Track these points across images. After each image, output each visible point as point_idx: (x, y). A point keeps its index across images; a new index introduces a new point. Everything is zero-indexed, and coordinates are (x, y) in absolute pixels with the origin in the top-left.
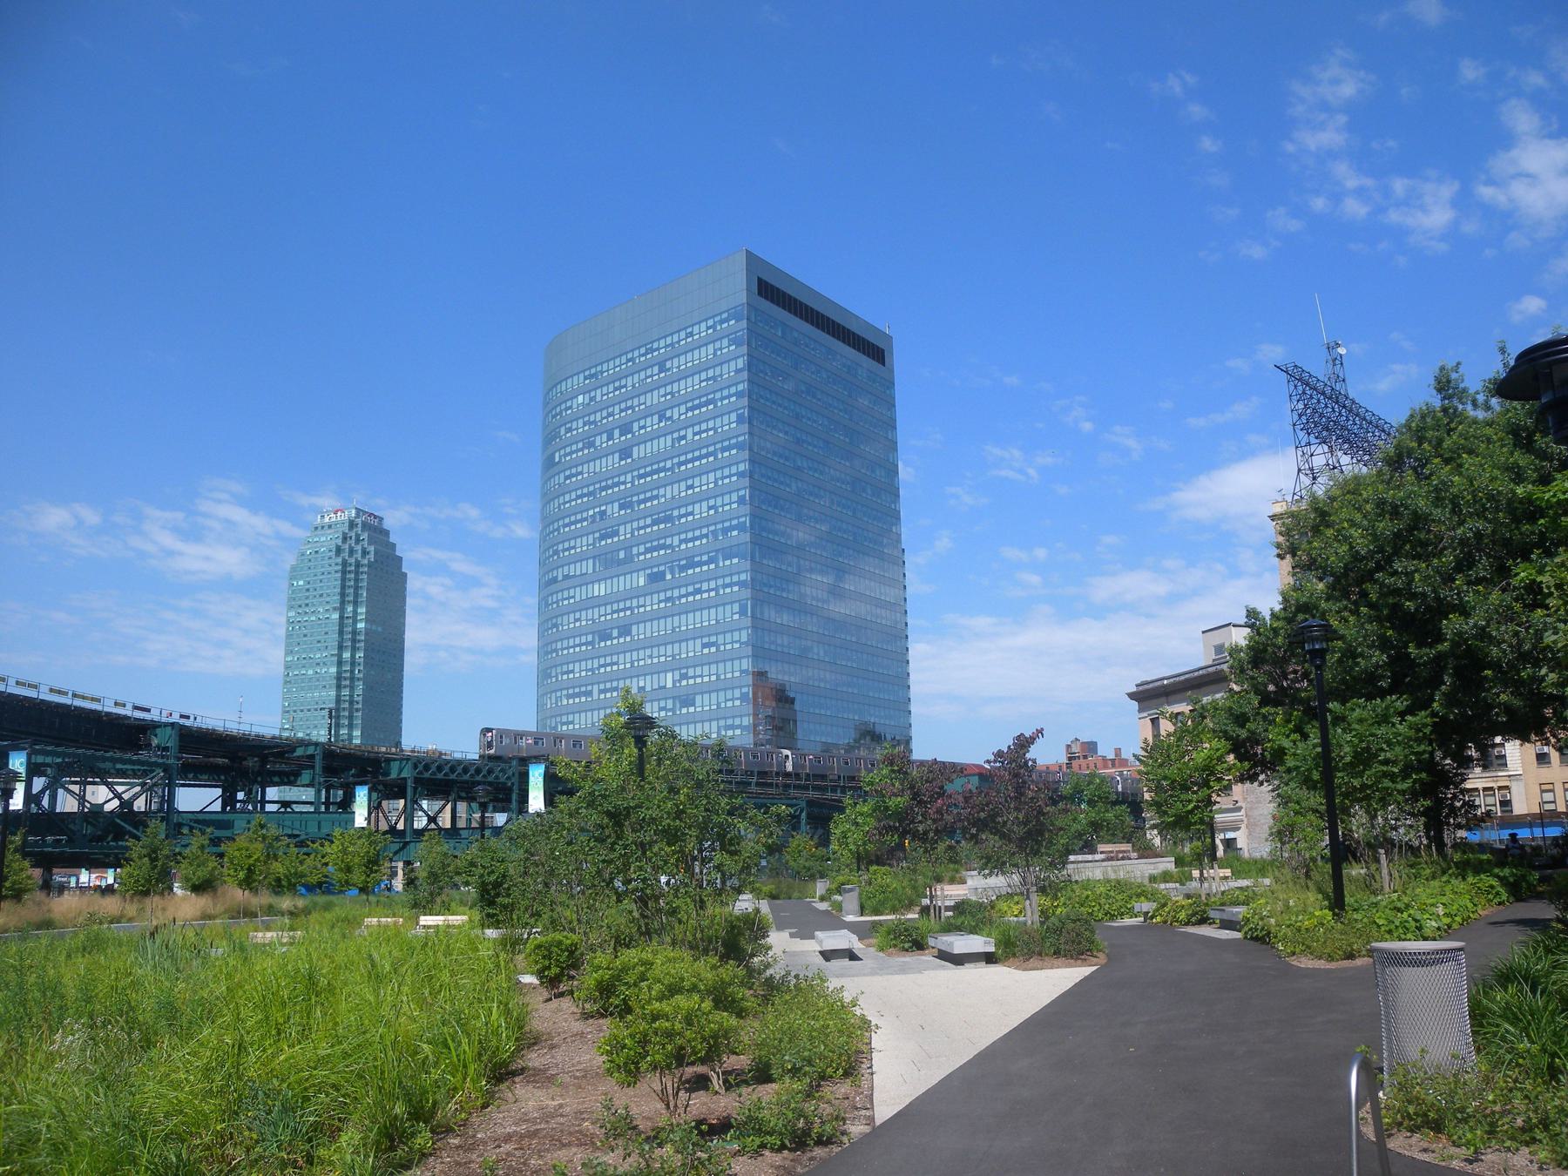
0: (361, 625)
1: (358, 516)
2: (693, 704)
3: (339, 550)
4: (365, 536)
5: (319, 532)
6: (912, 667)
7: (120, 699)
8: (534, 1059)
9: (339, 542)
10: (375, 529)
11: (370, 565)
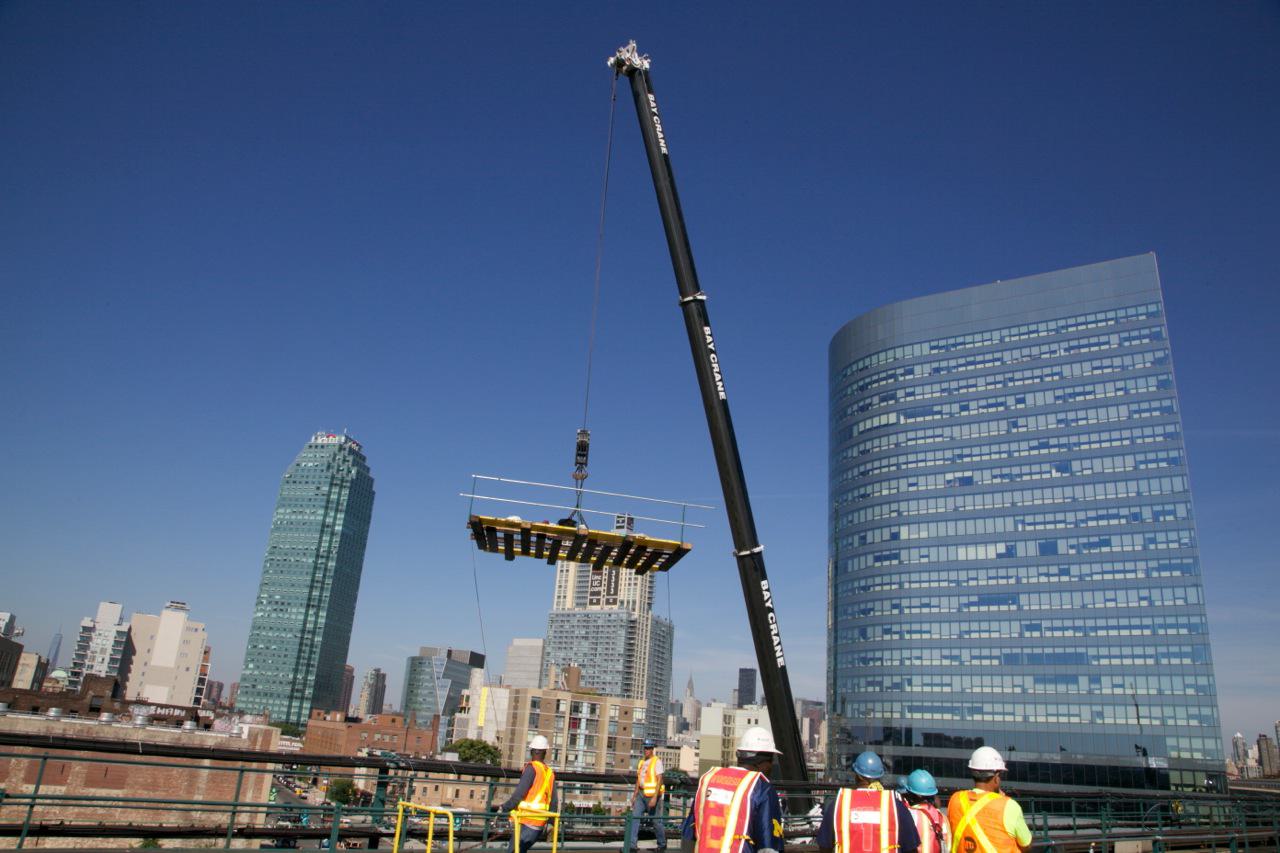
1: (346, 442)
2: (1015, 601)
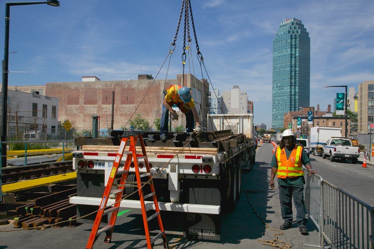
1: (294, 20)
3: (289, 32)
4: (297, 26)
5: (282, 27)
6: (311, 83)
7: (350, 106)
9: (289, 29)
11: (299, 35)
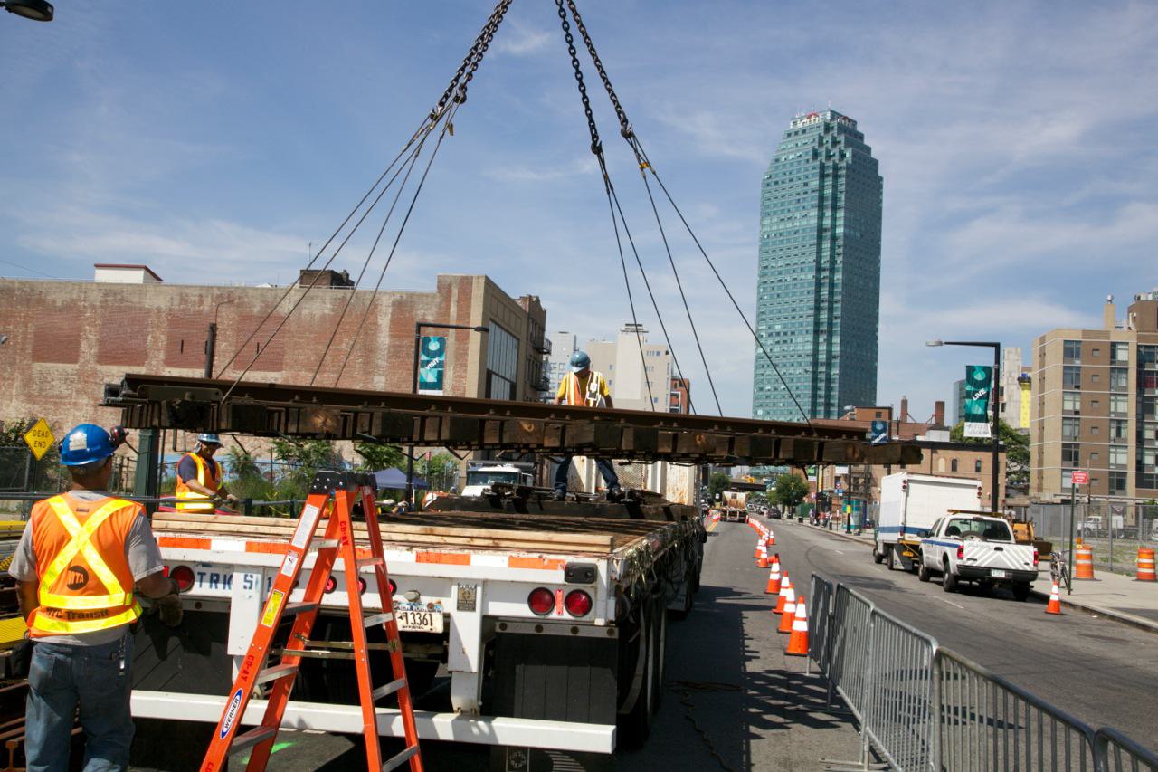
0: (839, 276)
1: (833, 118)
3: (816, 155)
4: (842, 138)
7: (1007, 408)
8: (214, 584)
9: (816, 145)
10: (848, 131)
11: (848, 167)
